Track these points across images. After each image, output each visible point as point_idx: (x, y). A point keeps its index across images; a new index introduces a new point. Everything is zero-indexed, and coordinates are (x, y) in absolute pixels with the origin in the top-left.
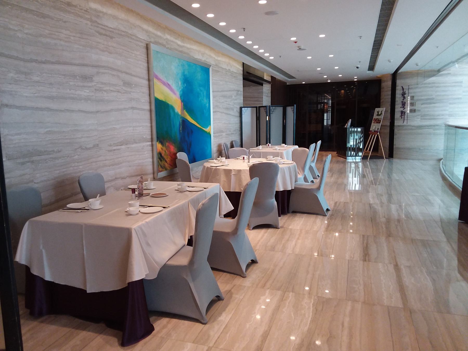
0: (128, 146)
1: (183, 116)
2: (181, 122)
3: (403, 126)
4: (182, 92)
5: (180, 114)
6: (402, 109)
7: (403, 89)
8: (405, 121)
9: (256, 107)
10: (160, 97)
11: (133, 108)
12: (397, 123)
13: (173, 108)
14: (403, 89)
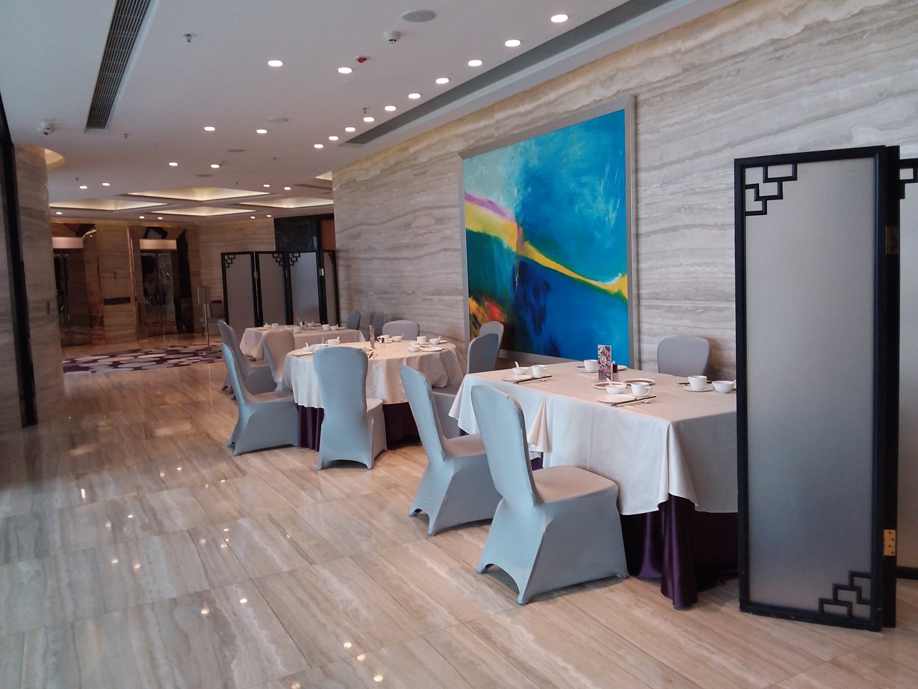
0: (441, 297)
1: (521, 253)
2: (517, 265)
4: (519, 208)
5: (514, 249)
9: (251, 253)
10: (476, 228)
11: (445, 250)
13: (498, 242)
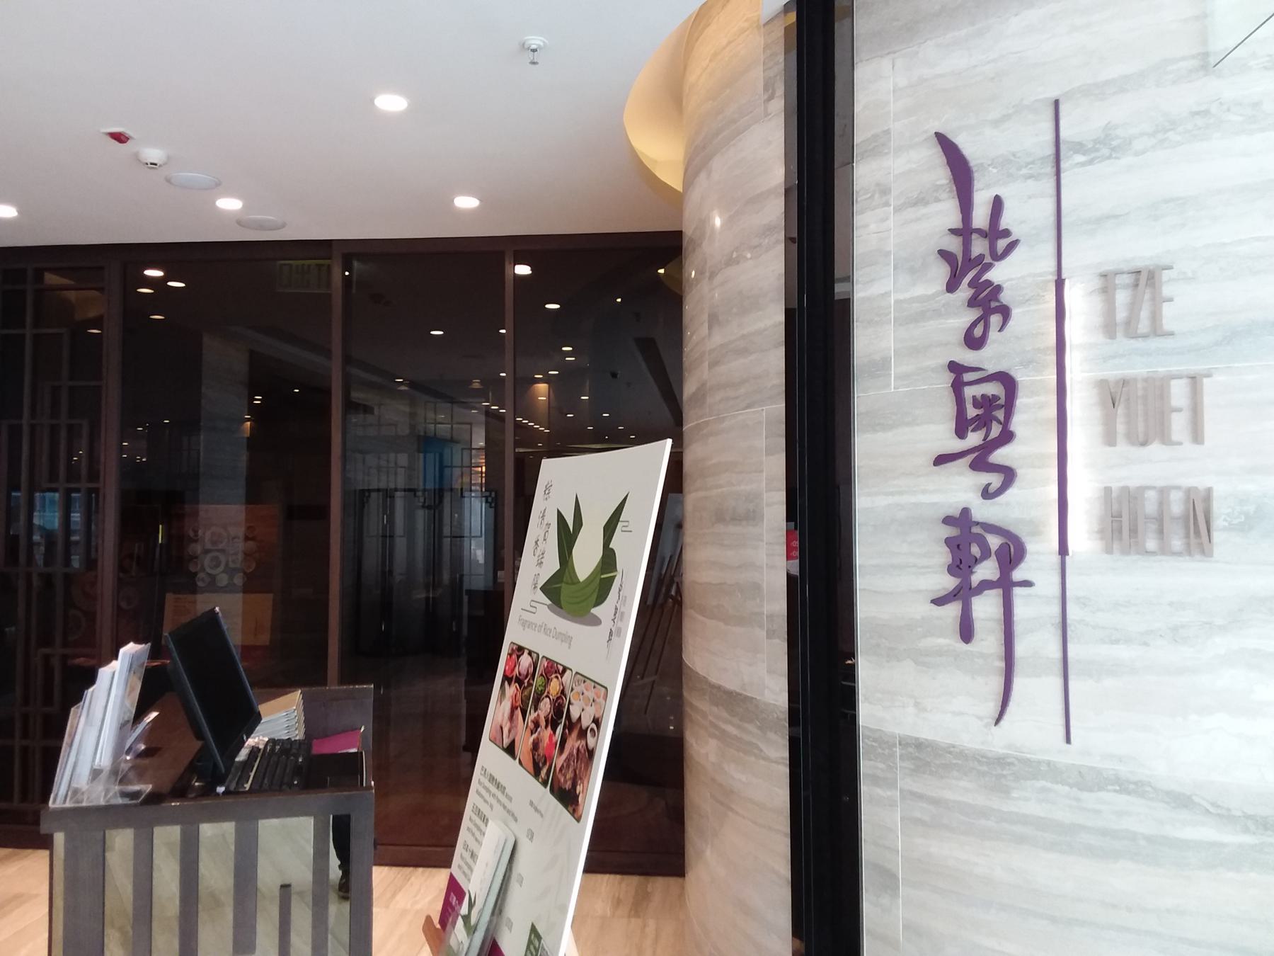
3: (999, 770)
6: (960, 489)
7: (961, 174)
8: (1036, 690)
12: (887, 701)
14: (961, 174)
